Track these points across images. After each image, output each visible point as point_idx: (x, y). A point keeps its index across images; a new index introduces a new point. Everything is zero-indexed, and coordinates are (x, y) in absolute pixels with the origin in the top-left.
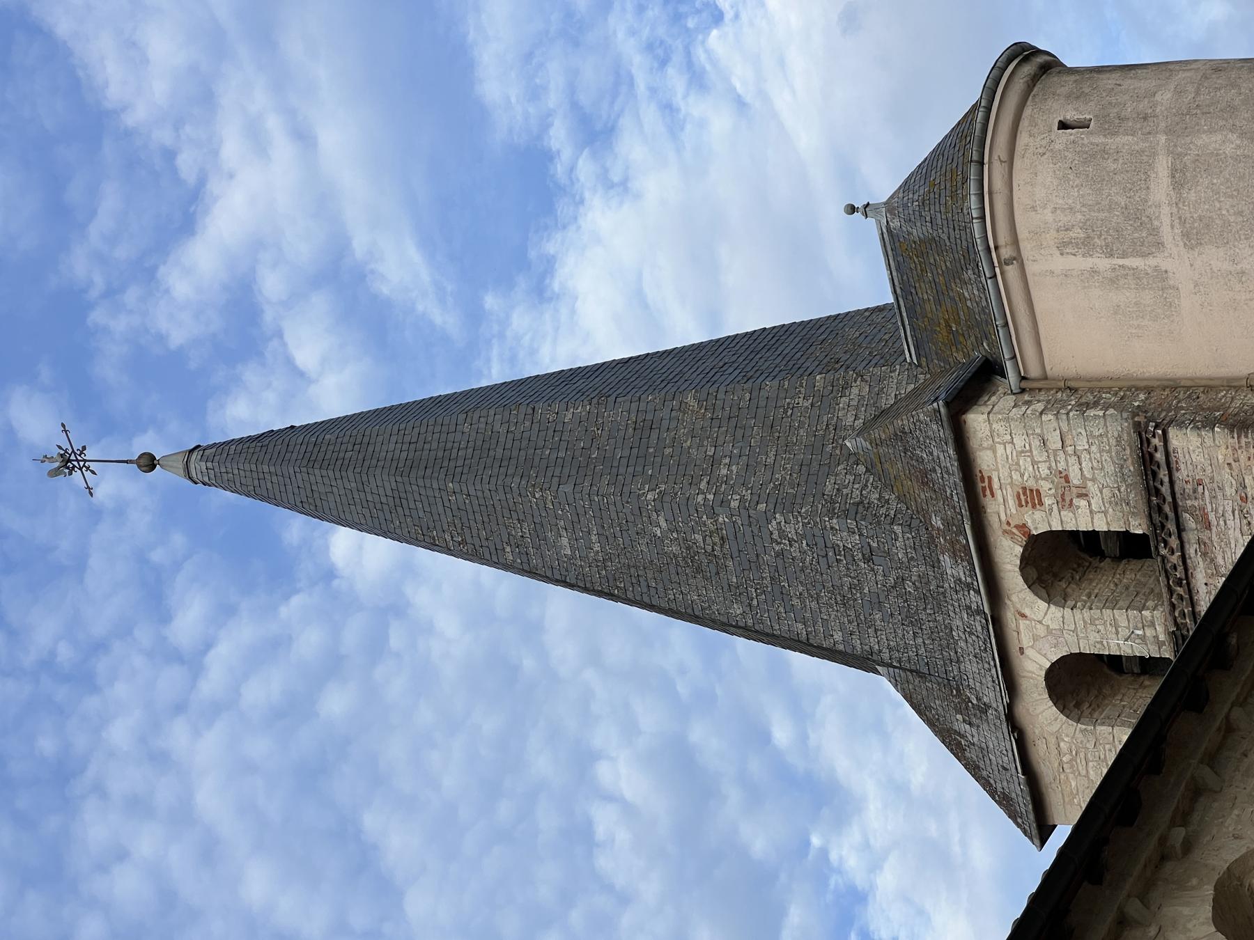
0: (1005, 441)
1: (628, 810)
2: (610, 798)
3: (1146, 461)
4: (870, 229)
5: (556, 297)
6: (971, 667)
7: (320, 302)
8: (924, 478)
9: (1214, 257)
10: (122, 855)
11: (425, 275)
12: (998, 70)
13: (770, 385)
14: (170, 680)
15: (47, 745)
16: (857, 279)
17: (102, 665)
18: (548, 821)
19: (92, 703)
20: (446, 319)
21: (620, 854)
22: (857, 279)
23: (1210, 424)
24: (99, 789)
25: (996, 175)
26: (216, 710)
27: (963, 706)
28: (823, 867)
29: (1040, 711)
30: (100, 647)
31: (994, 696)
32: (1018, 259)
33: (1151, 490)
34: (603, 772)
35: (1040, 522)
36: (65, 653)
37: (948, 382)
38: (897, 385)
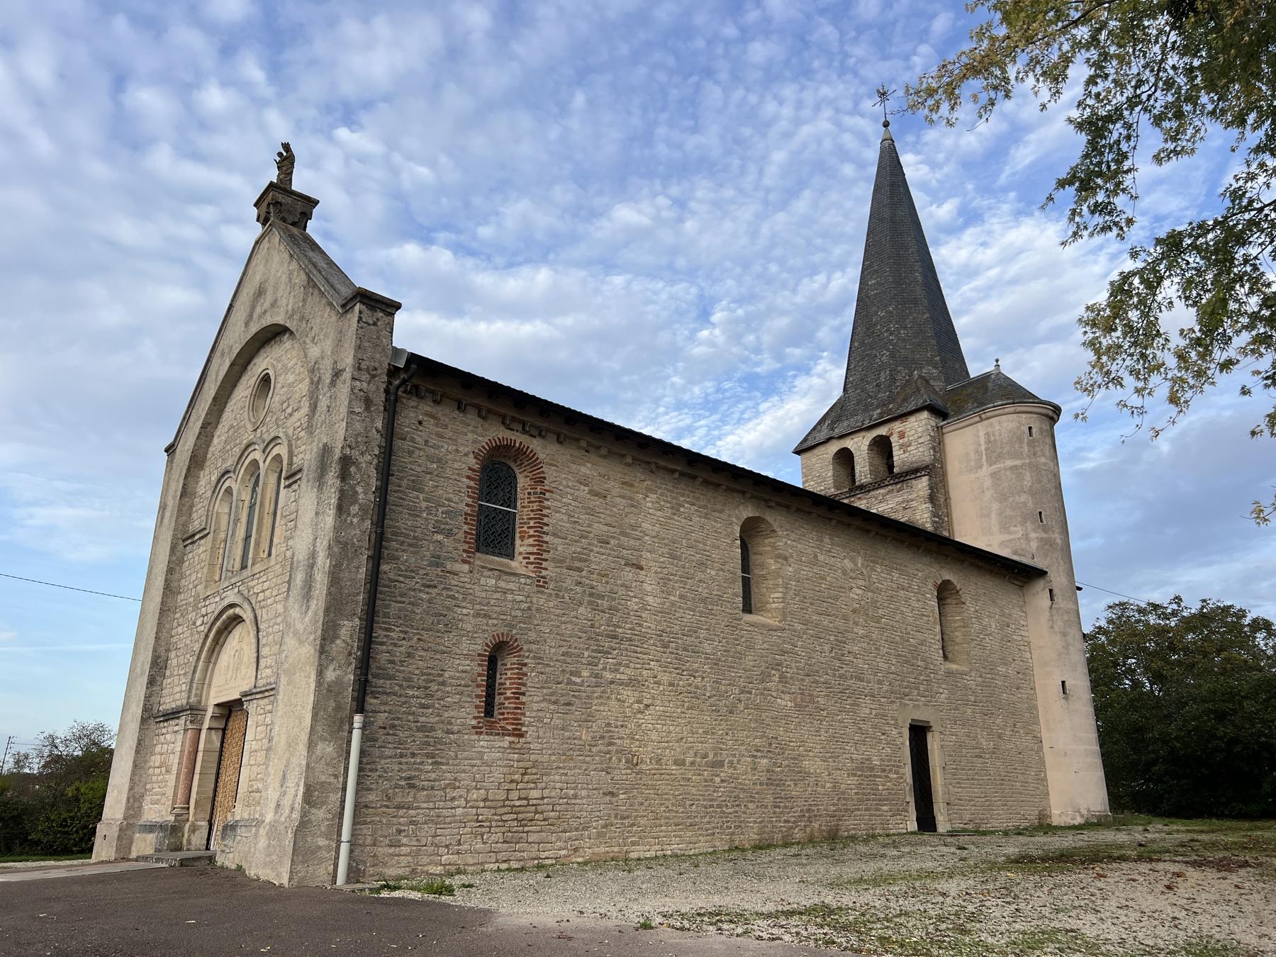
0: (918, 427)
1: (825, 286)
2: (829, 279)
3: (916, 470)
4: (990, 368)
5: (1017, 220)
6: (846, 423)
7: (1004, 127)
8: (905, 400)
9: (988, 482)
10: (781, 102)
11: (1020, 167)
12: (1049, 404)
13: (933, 342)
14: (847, 104)
15: (816, 64)
16: (975, 369)
17: (849, 77)
18: (817, 258)
19: (834, 77)
20: (1003, 179)
21: (810, 286)
22: (975, 369)
23: (931, 488)
24: (803, 88)
25: (1010, 409)
26: (838, 124)
27: (833, 423)
28: (816, 359)
29: (834, 447)
30: (856, 74)
31: (837, 432)
32: (982, 420)
33: (907, 473)
34: (838, 274)
35: (894, 439)
36: (852, 61)
37: (939, 403)
38: (938, 385)
